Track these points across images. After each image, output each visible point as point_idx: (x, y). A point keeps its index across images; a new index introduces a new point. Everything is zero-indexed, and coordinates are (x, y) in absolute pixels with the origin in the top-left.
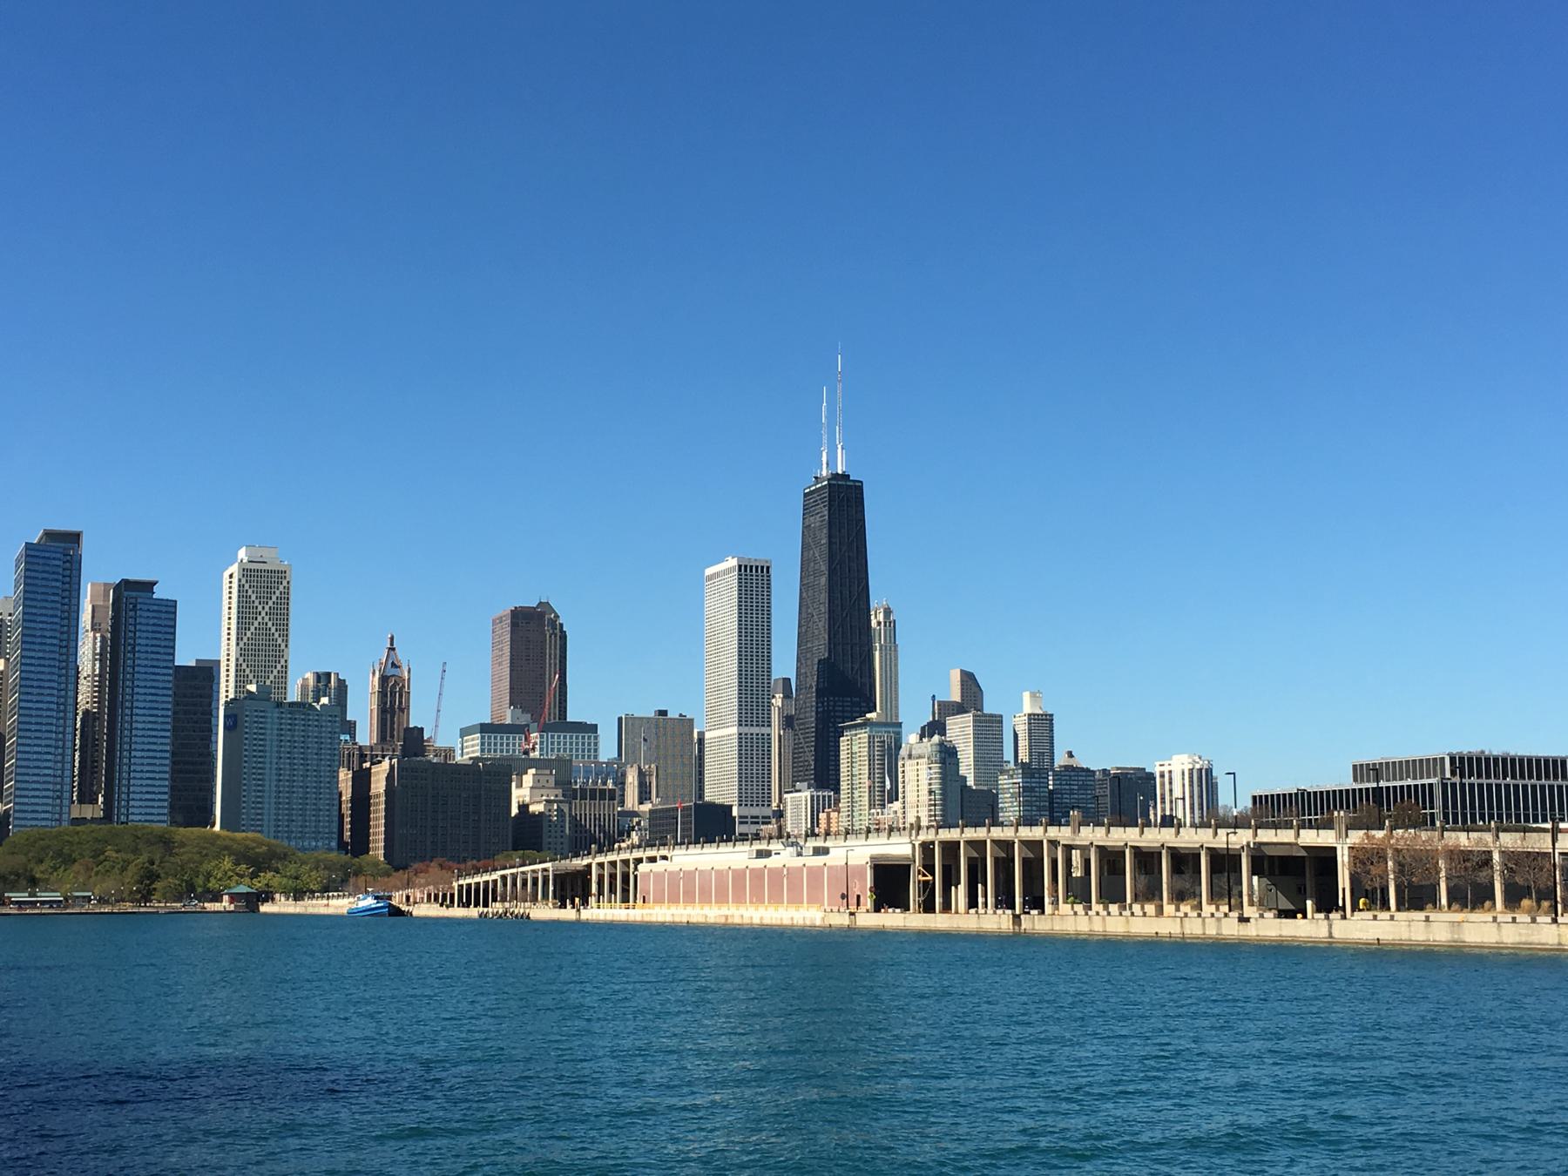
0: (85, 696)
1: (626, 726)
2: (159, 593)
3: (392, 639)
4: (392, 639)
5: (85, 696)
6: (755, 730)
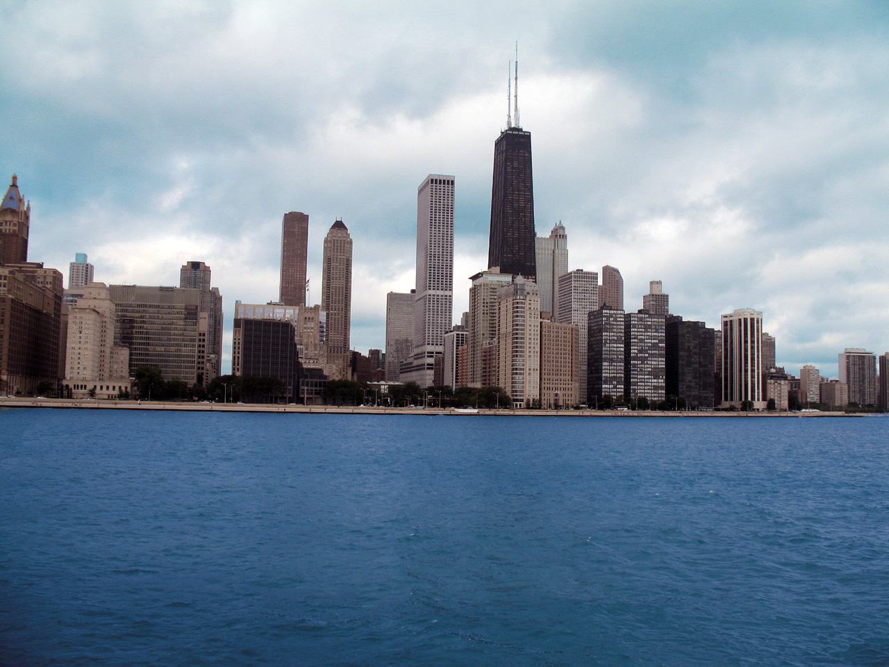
3: (15, 178)
4: (15, 178)
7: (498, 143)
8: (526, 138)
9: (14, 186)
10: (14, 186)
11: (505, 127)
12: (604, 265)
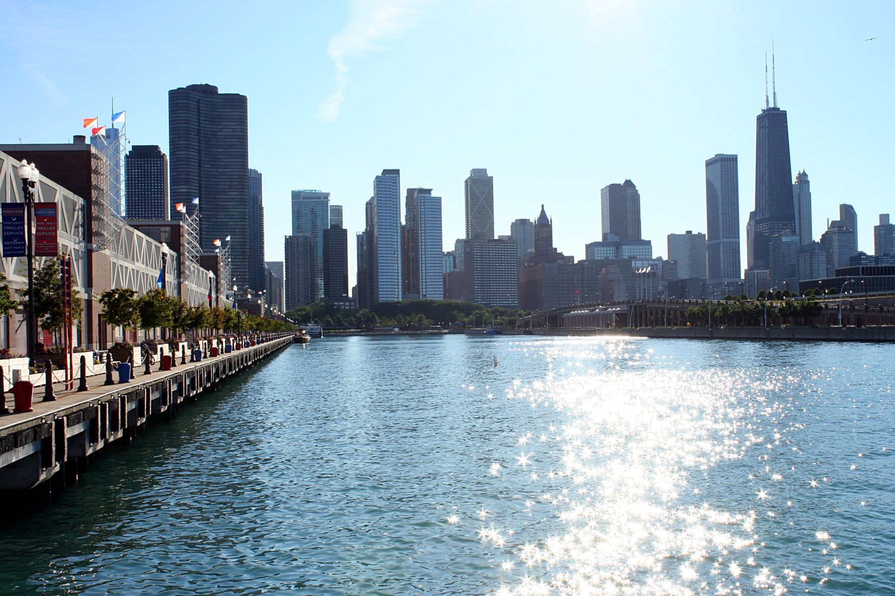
0: (353, 281)
1: (672, 238)
2: (434, 194)
5: (353, 281)
6: (731, 240)
7: (759, 118)
8: (784, 114)
9: (543, 212)
10: (543, 212)
11: (765, 107)
12: (712, 156)
